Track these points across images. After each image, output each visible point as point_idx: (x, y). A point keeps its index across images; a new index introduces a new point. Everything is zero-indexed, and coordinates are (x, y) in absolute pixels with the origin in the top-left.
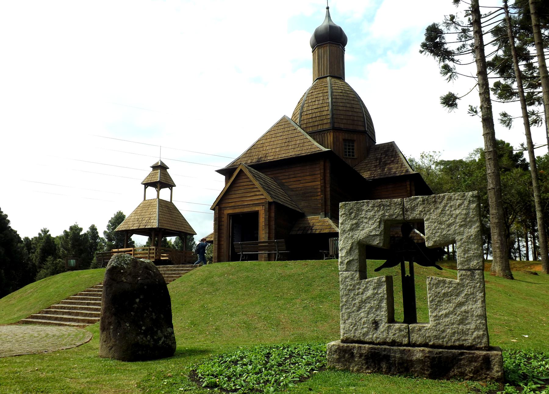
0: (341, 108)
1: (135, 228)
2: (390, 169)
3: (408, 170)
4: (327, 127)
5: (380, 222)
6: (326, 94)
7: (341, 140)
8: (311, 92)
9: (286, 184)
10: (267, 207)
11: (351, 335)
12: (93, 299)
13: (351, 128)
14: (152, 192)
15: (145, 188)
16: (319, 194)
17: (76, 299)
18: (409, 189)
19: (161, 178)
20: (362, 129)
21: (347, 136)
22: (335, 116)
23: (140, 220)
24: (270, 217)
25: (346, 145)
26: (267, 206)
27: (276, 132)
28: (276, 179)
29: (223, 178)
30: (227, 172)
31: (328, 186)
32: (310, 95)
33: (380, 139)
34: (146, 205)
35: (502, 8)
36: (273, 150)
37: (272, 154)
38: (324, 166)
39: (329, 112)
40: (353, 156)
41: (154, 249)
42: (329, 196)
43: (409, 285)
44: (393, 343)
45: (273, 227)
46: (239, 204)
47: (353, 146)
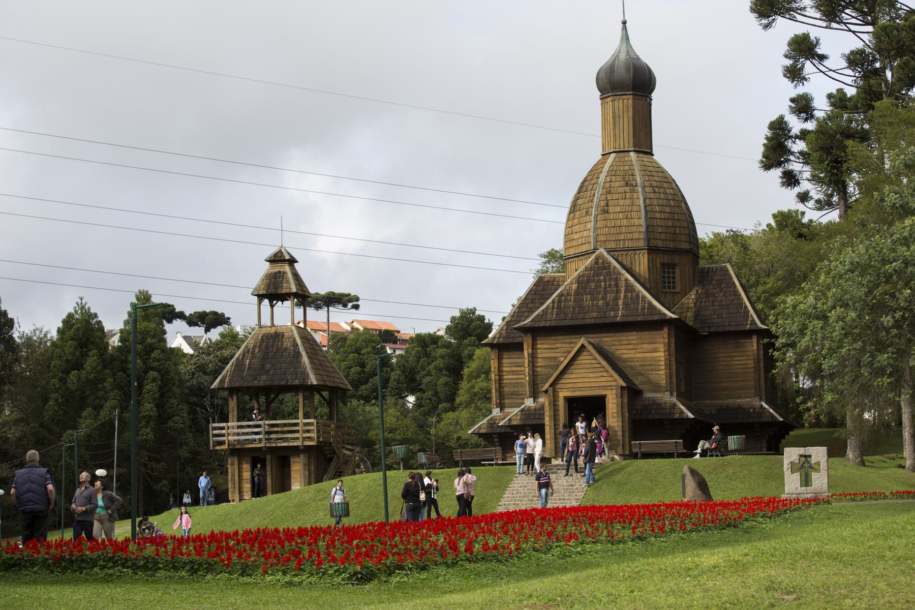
0: (658, 215)
7: (658, 265)
15: (260, 303)
21: (666, 259)
22: (650, 229)
25: (664, 272)
40: (674, 288)
47: (674, 273)
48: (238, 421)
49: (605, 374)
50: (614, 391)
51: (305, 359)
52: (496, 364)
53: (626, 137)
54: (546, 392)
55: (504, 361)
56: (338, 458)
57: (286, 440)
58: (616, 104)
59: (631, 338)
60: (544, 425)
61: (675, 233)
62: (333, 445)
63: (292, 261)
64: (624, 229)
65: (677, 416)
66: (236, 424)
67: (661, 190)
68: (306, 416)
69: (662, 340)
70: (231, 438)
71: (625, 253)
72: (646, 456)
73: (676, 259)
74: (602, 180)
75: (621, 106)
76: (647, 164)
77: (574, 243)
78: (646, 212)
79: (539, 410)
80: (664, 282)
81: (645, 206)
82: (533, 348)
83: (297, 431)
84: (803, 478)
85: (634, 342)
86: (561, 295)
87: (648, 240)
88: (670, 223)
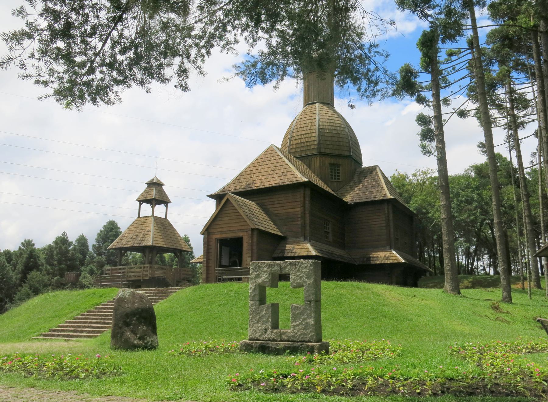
1: (128, 246)
2: (371, 193)
3: (386, 194)
4: (314, 152)
5: (269, 274)
6: (314, 121)
8: (300, 117)
9: (271, 210)
10: (250, 233)
11: (253, 336)
12: (95, 319)
13: (337, 153)
14: (146, 209)
15: (140, 205)
16: (300, 219)
17: (79, 319)
18: (386, 212)
19: (155, 194)
20: (347, 153)
22: (321, 142)
23: (134, 237)
24: (252, 242)
25: (332, 169)
26: (250, 232)
27: (263, 160)
28: (261, 205)
29: (214, 202)
30: (218, 197)
31: (307, 212)
32: (299, 120)
33: (366, 163)
34: (141, 221)
35: (469, 49)
36: (260, 178)
37: (258, 181)
38: (304, 194)
39: (316, 138)
40: (339, 179)
41: (148, 267)
42: (308, 222)
44: (274, 340)
45: (255, 251)
46: (226, 229)
47: (338, 170)
64: (306, 144)
73: (340, 161)
79: (111, 230)
80: (332, 175)
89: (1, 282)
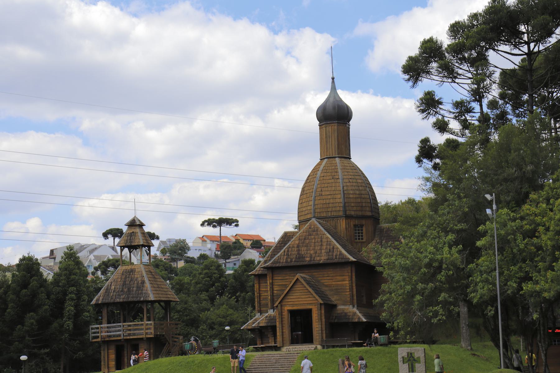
0: (351, 196)
4: (341, 213)
7: (352, 226)
13: (360, 214)
21: (357, 222)
31: (354, 285)
38: (351, 270)
39: (341, 200)
40: (362, 239)
42: (355, 293)
43: (412, 365)
45: (324, 320)
47: (362, 230)
48: (108, 323)
49: (311, 296)
50: (316, 306)
51: (148, 285)
52: (258, 287)
53: (333, 148)
54: (277, 306)
55: (262, 285)
56: (169, 343)
57: (134, 334)
58: (328, 129)
59: (329, 273)
60: (276, 326)
61: (362, 207)
62: (165, 336)
63: (141, 225)
65: (356, 320)
66: (106, 325)
67: (354, 181)
68: (149, 319)
69: (347, 274)
70: (103, 334)
71: (332, 219)
72: (333, 347)
73: (363, 222)
74: (318, 175)
75: (330, 130)
76: (346, 165)
77: (303, 213)
78: (344, 194)
81: (344, 191)
82: (272, 279)
83: (142, 329)
84: (410, 366)
85: (332, 275)
86: (289, 247)
87: (345, 211)
88: (359, 200)
89: (428, 366)
